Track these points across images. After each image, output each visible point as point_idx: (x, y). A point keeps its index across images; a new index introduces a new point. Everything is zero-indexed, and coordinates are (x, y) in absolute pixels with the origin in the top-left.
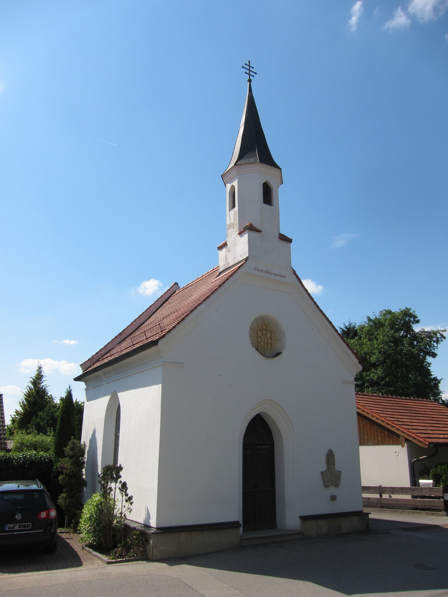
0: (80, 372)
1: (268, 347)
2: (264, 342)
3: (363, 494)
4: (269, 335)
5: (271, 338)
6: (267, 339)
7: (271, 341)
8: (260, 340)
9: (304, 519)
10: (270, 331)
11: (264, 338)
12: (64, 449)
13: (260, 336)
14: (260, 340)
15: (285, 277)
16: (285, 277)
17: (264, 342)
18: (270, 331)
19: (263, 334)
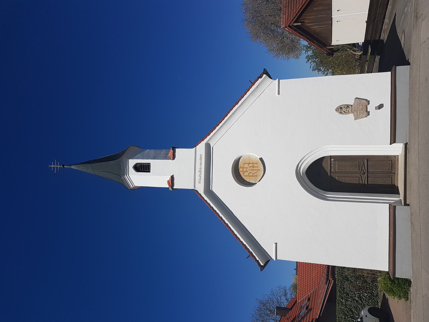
0: (403, 300)
1: (256, 167)
2: (252, 170)
3: (379, 57)
4: (246, 166)
5: (249, 164)
6: (250, 167)
7: (251, 163)
8: (251, 174)
9: (393, 140)
10: (244, 165)
11: (249, 170)
12: (172, 171)
13: (249, 174)
14: (251, 174)
15: (279, 94)
16: (279, 94)
17: (252, 170)
18: (244, 165)
19: (246, 171)
